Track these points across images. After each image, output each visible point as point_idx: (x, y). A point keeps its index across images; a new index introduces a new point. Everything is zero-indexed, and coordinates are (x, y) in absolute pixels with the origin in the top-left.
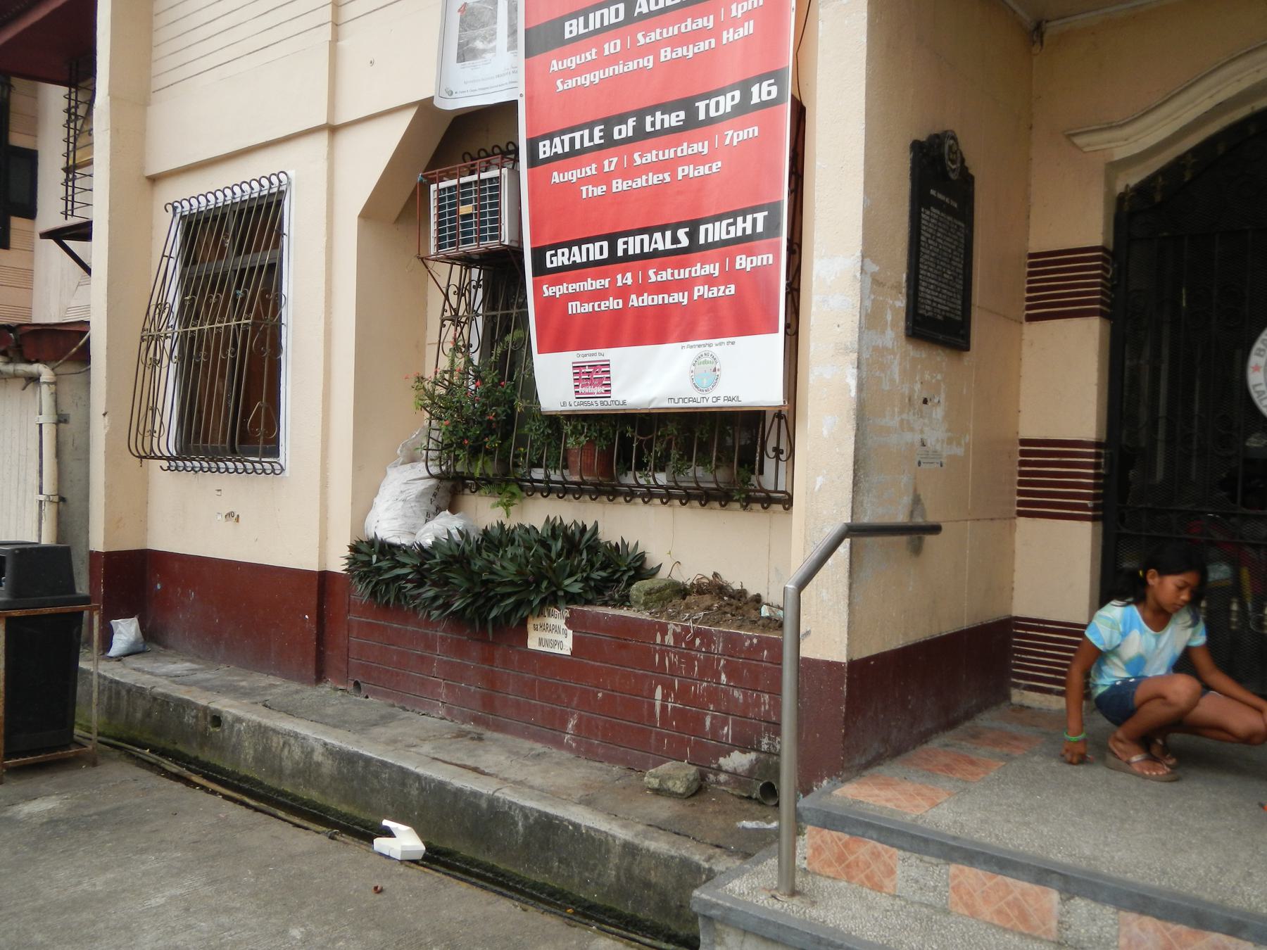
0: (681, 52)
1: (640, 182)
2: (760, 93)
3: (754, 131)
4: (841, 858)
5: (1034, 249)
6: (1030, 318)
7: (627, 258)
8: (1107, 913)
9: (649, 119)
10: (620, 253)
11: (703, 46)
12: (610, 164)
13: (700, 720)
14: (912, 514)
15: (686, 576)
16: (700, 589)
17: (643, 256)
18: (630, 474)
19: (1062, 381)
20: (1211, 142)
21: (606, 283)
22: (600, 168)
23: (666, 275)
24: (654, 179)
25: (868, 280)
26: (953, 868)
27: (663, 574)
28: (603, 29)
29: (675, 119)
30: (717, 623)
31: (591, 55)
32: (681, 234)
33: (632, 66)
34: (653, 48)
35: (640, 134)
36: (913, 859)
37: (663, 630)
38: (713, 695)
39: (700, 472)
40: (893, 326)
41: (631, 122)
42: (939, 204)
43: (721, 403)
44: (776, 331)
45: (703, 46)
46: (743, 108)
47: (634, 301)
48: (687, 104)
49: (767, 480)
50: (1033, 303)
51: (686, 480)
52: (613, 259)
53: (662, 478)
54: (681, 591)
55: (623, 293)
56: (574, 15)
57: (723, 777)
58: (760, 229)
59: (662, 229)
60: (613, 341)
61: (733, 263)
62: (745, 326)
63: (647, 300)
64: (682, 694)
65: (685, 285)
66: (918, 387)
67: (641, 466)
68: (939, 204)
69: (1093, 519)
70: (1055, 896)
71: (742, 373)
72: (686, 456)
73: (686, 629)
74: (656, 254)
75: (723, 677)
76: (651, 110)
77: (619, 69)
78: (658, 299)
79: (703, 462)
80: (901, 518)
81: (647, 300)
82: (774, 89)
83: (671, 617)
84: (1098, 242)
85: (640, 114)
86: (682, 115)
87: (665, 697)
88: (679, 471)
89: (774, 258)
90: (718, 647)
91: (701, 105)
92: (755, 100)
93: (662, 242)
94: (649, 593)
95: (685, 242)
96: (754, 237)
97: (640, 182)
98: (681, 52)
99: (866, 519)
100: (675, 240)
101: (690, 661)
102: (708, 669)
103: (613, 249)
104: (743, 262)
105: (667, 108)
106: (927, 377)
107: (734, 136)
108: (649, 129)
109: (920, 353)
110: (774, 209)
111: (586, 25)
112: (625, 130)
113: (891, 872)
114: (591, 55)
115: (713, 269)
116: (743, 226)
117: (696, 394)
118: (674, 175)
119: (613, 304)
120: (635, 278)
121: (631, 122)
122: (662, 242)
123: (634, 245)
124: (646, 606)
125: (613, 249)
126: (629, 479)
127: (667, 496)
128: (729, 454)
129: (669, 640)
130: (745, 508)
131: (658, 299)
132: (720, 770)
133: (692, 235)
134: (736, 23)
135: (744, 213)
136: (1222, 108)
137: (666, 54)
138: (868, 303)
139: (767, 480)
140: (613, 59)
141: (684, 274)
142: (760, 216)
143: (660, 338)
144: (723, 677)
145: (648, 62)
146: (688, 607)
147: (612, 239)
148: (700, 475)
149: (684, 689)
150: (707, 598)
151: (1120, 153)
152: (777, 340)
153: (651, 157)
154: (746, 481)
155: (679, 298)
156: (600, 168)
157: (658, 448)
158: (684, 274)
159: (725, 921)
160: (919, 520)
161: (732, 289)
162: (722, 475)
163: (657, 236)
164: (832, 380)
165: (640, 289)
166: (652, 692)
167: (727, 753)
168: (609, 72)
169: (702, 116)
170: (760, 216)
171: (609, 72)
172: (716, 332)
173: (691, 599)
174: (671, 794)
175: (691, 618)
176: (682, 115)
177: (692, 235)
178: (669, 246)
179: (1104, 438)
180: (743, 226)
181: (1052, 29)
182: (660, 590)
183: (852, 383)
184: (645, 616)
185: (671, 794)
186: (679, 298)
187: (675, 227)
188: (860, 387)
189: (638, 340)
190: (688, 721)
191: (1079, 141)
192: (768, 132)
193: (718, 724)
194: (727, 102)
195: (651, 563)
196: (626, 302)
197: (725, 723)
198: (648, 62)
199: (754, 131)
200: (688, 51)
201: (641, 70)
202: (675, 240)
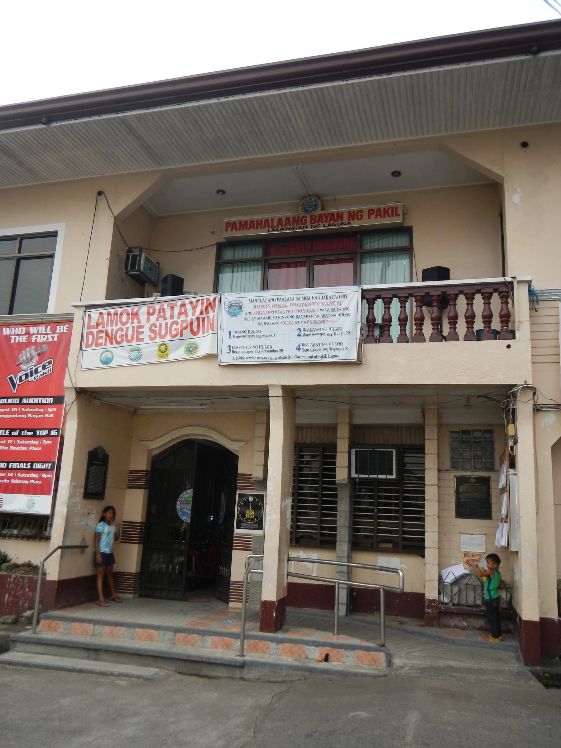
0: (34, 416)
1: (18, 448)
2: (54, 433)
3: (50, 442)
4: (49, 626)
5: (132, 467)
6: (128, 488)
7: (12, 469)
8: (101, 627)
9: (23, 432)
10: (10, 467)
11: (40, 416)
12: (10, 441)
13: (18, 603)
14: (82, 543)
15: (20, 562)
16: (23, 565)
17: (16, 469)
18: (5, 530)
19: (134, 506)
20: (174, 445)
21: (5, 475)
22: (7, 442)
23: (23, 475)
24: (22, 448)
25: (72, 487)
26: (73, 624)
27: (13, 561)
28: (12, 404)
29: (31, 433)
30: (27, 574)
31: (8, 410)
32: (29, 464)
33: (19, 416)
34: (26, 413)
35: (20, 435)
36: (65, 623)
37: (10, 577)
38: (23, 595)
39: (27, 530)
40: (79, 496)
41: (18, 431)
42: (96, 464)
43: (34, 512)
44: (50, 495)
45: (40, 416)
46: (48, 436)
47: (13, 481)
48: (34, 430)
49: (46, 534)
50: (129, 484)
51: (23, 533)
52: (7, 468)
53: (15, 532)
54: (17, 566)
55: (10, 478)
56: (4, 398)
57: (23, 619)
58: (49, 468)
59: (24, 462)
60: (5, 492)
61: (41, 475)
62: (43, 493)
63: (16, 481)
64: (14, 596)
65: (28, 479)
66: (86, 510)
67: (9, 528)
68: (96, 464)
69: (139, 543)
70: (92, 625)
71: (40, 505)
72: (23, 526)
73: (17, 576)
74: (21, 469)
75: (27, 590)
76: (24, 430)
77: (16, 416)
78: (20, 482)
79: (29, 527)
80: (78, 544)
81: (16, 481)
82: (57, 433)
83: (13, 573)
84: (145, 469)
85: (21, 430)
86: (32, 433)
87: (8, 597)
88: (21, 530)
89: (51, 476)
90: (26, 581)
91: (38, 431)
92: (52, 434)
93: (23, 466)
94: (7, 567)
95: (29, 467)
96: (47, 470)
97: (18, 448)
98: (34, 416)
99: (67, 544)
100: (27, 466)
101: (17, 586)
102: (23, 588)
103: (8, 465)
104: (44, 476)
105: (29, 430)
106: (90, 507)
107: (46, 442)
108: (22, 434)
109: (88, 502)
110: (53, 463)
111: (7, 401)
112: (16, 433)
113: (59, 627)
114: (8, 410)
115: (36, 476)
116: (45, 466)
117: (28, 510)
118: (28, 448)
119: (6, 481)
120: (14, 474)
121: (18, 431)
122: (23, 466)
123: (14, 465)
124: (6, 570)
125: (8, 465)
126: (5, 532)
127: (17, 537)
128: (35, 527)
129: (12, 580)
130: (40, 541)
131: (20, 482)
132: (23, 617)
133: (32, 466)
134: (50, 413)
135: (46, 463)
136: (173, 440)
137: (30, 416)
138: (71, 492)
139: (46, 534)
140: (14, 413)
141: (28, 476)
142: (50, 465)
143: (19, 492)
144: (27, 590)
145: (24, 416)
146: (19, 570)
147: (8, 463)
148: (27, 531)
149: (15, 594)
150: (25, 568)
151: (152, 447)
152: (50, 498)
153: (22, 442)
154: (41, 533)
155: (26, 482)
156: (7, 442)
157: (15, 523)
158: (28, 476)
159: (17, 641)
160: (84, 544)
161: (40, 482)
162: (34, 531)
163: (22, 464)
164: (61, 510)
165: (15, 478)
166: (5, 595)
167: (25, 611)
168: (13, 416)
169: (38, 435)
170: (50, 465)
171: (13, 416)
172: (35, 493)
173: (20, 568)
174: (7, 623)
175: (19, 574)
176: (32, 433)
177: (32, 466)
178: (25, 467)
179: (144, 521)
180: (45, 466)
181: (139, 412)
182: (11, 566)
183: (65, 511)
184: (5, 573)
185: (7, 623)
186: (26, 482)
187: (27, 463)
188: (68, 512)
189: (13, 492)
190: (15, 603)
191: (143, 442)
192: (54, 443)
193: (23, 604)
194: (45, 433)
195: (9, 558)
196: (10, 481)
197: (26, 602)
198: (24, 416)
199: (50, 442)
200: (36, 417)
201: (22, 418)
202: (27, 466)
